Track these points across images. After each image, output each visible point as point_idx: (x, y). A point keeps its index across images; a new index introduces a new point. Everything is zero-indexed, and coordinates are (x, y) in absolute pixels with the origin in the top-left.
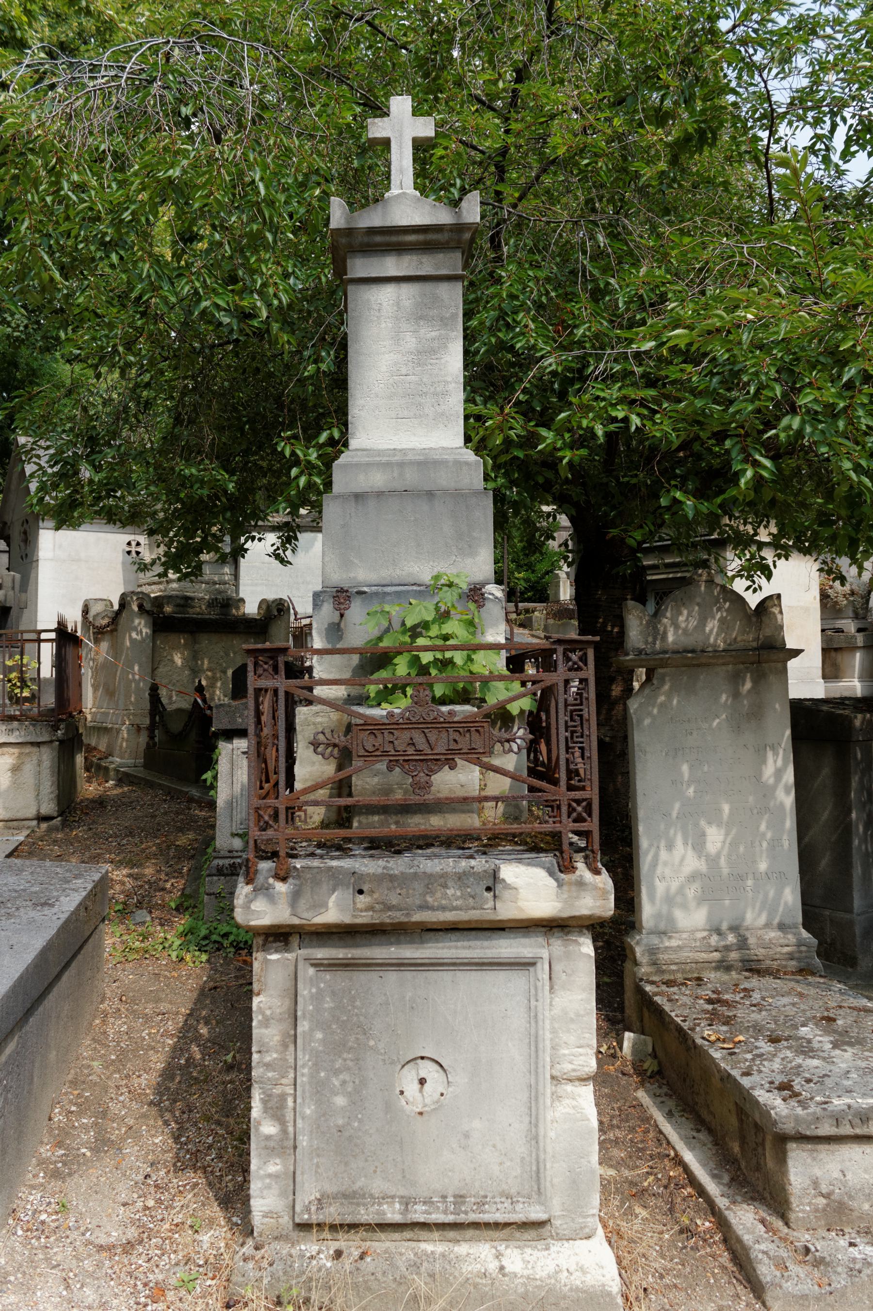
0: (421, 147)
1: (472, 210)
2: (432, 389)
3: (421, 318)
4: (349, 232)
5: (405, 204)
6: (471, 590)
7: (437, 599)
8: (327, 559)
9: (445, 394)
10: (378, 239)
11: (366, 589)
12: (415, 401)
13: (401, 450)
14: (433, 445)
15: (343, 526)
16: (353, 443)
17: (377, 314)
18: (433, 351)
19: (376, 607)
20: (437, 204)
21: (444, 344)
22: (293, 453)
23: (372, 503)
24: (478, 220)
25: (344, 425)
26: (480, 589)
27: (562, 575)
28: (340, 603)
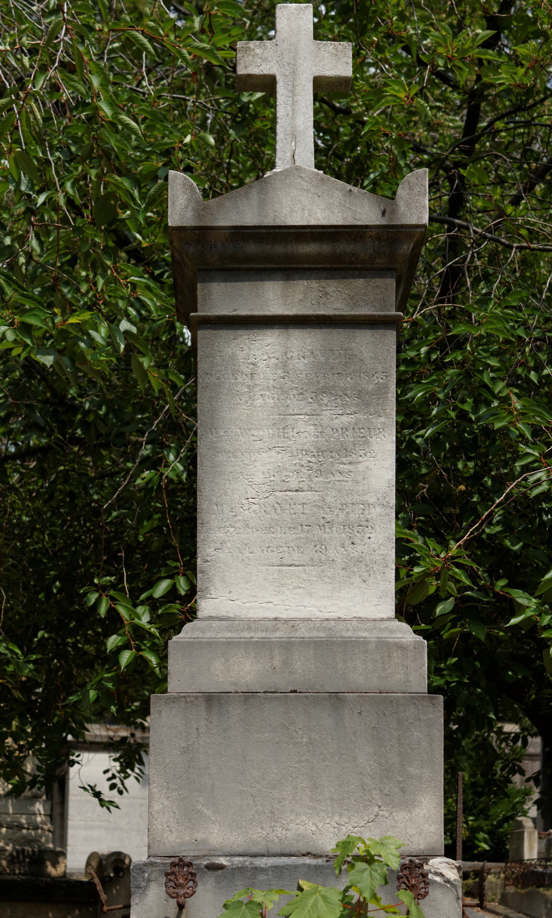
0: (326, 91)
1: (415, 202)
2: (342, 517)
3: (324, 390)
4: (200, 234)
5: (301, 194)
6: (404, 867)
7: (345, 882)
8: (156, 807)
9: (364, 525)
10: (252, 248)
11: (223, 861)
12: (311, 536)
13: (287, 621)
14: (341, 614)
15: (186, 751)
16: (206, 606)
17: (248, 381)
18: (344, 450)
19: (239, 894)
20: (355, 189)
21: (363, 436)
22: (112, 612)
23: (235, 712)
24: (425, 220)
25: (191, 568)
26: (421, 866)
27: (528, 824)
28: (177, 886)
